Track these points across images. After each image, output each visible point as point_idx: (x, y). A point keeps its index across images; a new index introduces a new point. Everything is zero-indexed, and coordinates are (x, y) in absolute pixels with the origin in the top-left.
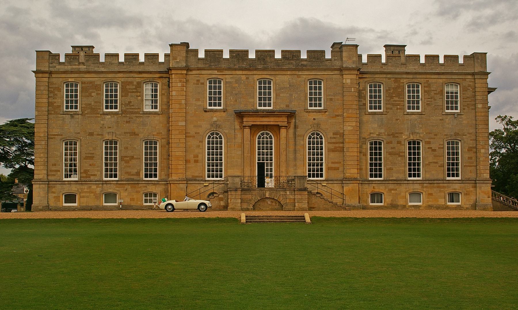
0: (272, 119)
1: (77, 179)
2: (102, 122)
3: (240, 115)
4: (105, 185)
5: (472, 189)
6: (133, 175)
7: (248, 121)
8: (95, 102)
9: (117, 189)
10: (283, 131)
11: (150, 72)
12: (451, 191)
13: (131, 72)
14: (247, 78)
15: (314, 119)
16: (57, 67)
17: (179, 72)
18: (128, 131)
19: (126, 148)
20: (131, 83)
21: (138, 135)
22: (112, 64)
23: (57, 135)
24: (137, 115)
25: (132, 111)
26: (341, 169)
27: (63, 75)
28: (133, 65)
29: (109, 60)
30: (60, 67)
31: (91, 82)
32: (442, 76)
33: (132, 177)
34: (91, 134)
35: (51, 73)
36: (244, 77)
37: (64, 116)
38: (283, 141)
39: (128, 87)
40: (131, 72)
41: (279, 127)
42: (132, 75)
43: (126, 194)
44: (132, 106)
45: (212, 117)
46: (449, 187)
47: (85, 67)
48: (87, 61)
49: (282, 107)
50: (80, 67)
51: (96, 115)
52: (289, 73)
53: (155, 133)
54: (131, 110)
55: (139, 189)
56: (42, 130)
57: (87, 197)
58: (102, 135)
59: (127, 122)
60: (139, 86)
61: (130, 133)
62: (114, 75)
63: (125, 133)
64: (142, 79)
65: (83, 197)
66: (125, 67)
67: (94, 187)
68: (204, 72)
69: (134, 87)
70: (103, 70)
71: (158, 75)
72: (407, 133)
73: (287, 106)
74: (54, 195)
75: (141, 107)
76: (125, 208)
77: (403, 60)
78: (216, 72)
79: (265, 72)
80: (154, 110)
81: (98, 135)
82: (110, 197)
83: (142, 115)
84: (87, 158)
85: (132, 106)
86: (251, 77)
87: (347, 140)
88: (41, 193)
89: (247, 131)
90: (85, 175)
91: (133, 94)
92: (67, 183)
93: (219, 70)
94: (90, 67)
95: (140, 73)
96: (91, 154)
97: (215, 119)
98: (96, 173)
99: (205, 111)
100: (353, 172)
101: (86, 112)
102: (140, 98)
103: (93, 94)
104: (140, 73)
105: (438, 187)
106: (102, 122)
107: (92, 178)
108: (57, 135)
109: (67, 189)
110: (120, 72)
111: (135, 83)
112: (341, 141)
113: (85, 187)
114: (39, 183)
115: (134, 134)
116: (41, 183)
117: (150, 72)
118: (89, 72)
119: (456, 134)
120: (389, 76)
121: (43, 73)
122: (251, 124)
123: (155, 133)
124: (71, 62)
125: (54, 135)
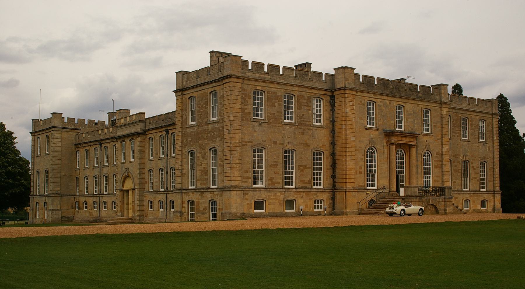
0: (408, 139)
1: (263, 186)
2: (283, 132)
3: (388, 134)
4: (287, 192)
5: (492, 198)
6: (306, 183)
7: (395, 140)
8: (278, 112)
9: (296, 196)
10: (414, 150)
11: (318, 89)
12: (256, 199)
13: (305, 87)
14: (390, 103)
15: (427, 141)
16: (247, 74)
17: (351, 92)
18: (302, 142)
19: (301, 158)
20: (303, 97)
21: (309, 146)
22: (290, 77)
23: (249, 142)
24: (309, 128)
25: (303, 124)
26: (440, 181)
27: (253, 83)
28: (305, 81)
29: (287, 73)
30: (249, 74)
31: (274, 93)
32: (478, 114)
33: (306, 185)
34: (275, 143)
35: (243, 79)
36: (388, 102)
37: (254, 123)
38: (414, 158)
39: (301, 101)
40: (305, 87)
41: (410, 146)
42: (305, 90)
43: (302, 201)
44: (305, 118)
45: (370, 134)
46: (482, 196)
47: (269, 77)
48: (271, 71)
49: (409, 130)
50: (266, 76)
51: (278, 125)
52: (413, 102)
53: (321, 145)
54: (304, 123)
55: (311, 197)
56: (237, 136)
57: (274, 204)
58: (283, 144)
59: (302, 133)
60: (309, 100)
61: (303, 144)
62: (292, 87)
63: (300, 143)
64: (312, 95)
65: (270, 204)
66: (299, 81)
67: (278, 194)
68: (365, 94)
69: (306, 101)
70: (283, 81)
71: (323, 92)
72: (462, 155)
73: (412, 129)
74: (247, 202)
75: (311, 121)
76: (299, 214)
77: (263, 72)
78: (372, 96)
79: (401, 100)
80: (318, 124)
81: (280, 144)
82: (290, 203)
83: (312, 128)
84: (272, 166)
85: (305, 118)
86: (392, 103)
87: (444, 159)
88: (238, 200)
89: (393, 148)
90: (270, 182)
91: (306, 108)
92: (258, 190)
93: (374, 94)
94: (274, 78)
95: (311, 88)
96: (275, 162)
97: (372, 136)
98: (279, 180)
99: (366, 129)
100: (237, 181)
101: (271, 121)
102: (310, 112)
103: (276, 104)
104: (311, 88)
105: (477, 196)
106: (283, 132)
107: (277, 185)
108: (249, 142)
109: (258, 196)
110: (297, 86)
111: (306, 98)
112: (440, 159)
113: (272, 194)
114: (236, 189)
115: (307, 145)
116: (238, 189)
117: (318, 89)
118: (274, 83)
119: (485, 158)
120: (454, 111)
121: (238, 78)
122: (397, 142)
123: (321, 145)
124: (258, 70)
125: (246, 142)
